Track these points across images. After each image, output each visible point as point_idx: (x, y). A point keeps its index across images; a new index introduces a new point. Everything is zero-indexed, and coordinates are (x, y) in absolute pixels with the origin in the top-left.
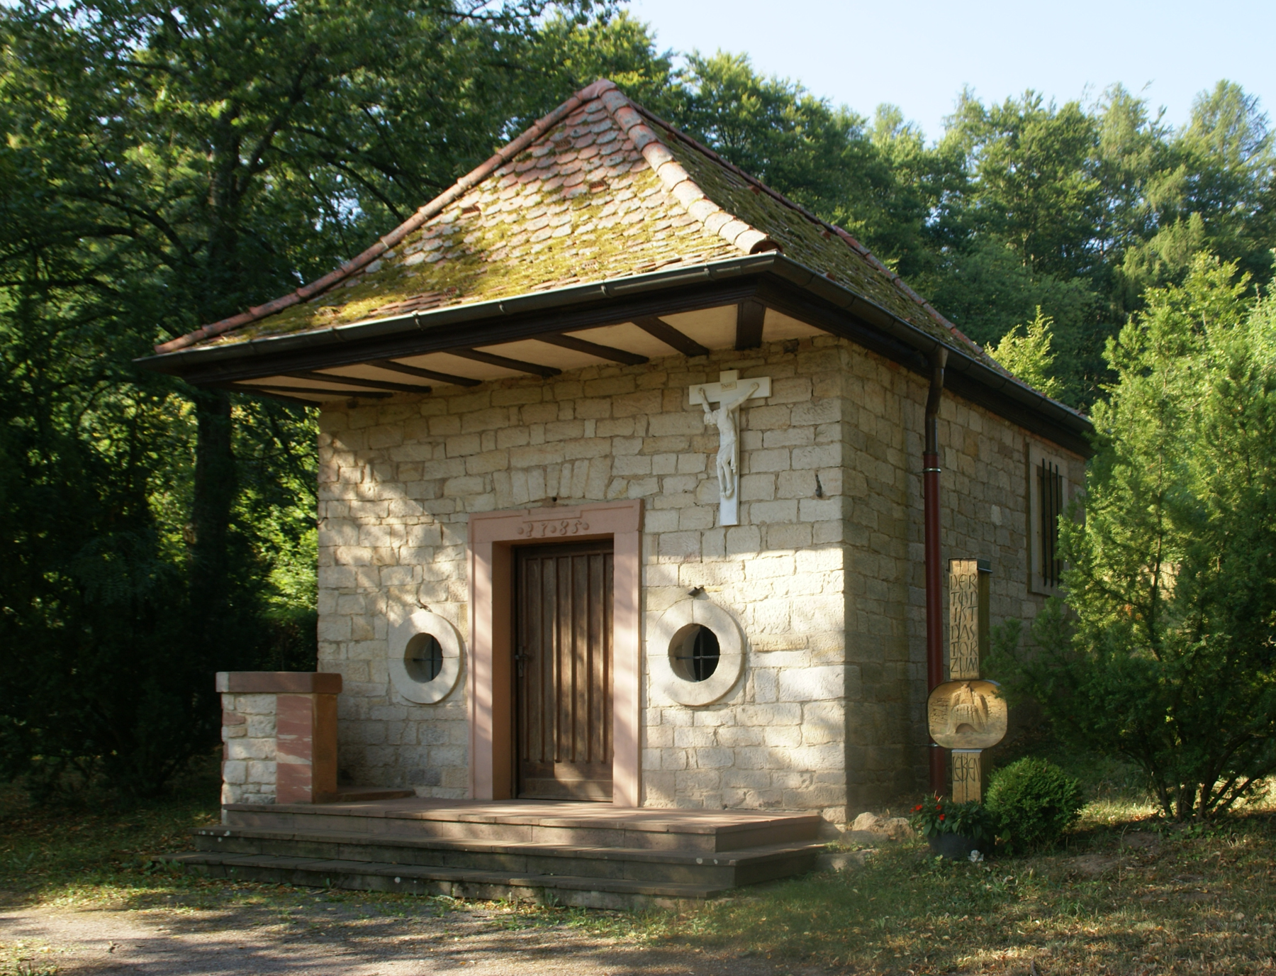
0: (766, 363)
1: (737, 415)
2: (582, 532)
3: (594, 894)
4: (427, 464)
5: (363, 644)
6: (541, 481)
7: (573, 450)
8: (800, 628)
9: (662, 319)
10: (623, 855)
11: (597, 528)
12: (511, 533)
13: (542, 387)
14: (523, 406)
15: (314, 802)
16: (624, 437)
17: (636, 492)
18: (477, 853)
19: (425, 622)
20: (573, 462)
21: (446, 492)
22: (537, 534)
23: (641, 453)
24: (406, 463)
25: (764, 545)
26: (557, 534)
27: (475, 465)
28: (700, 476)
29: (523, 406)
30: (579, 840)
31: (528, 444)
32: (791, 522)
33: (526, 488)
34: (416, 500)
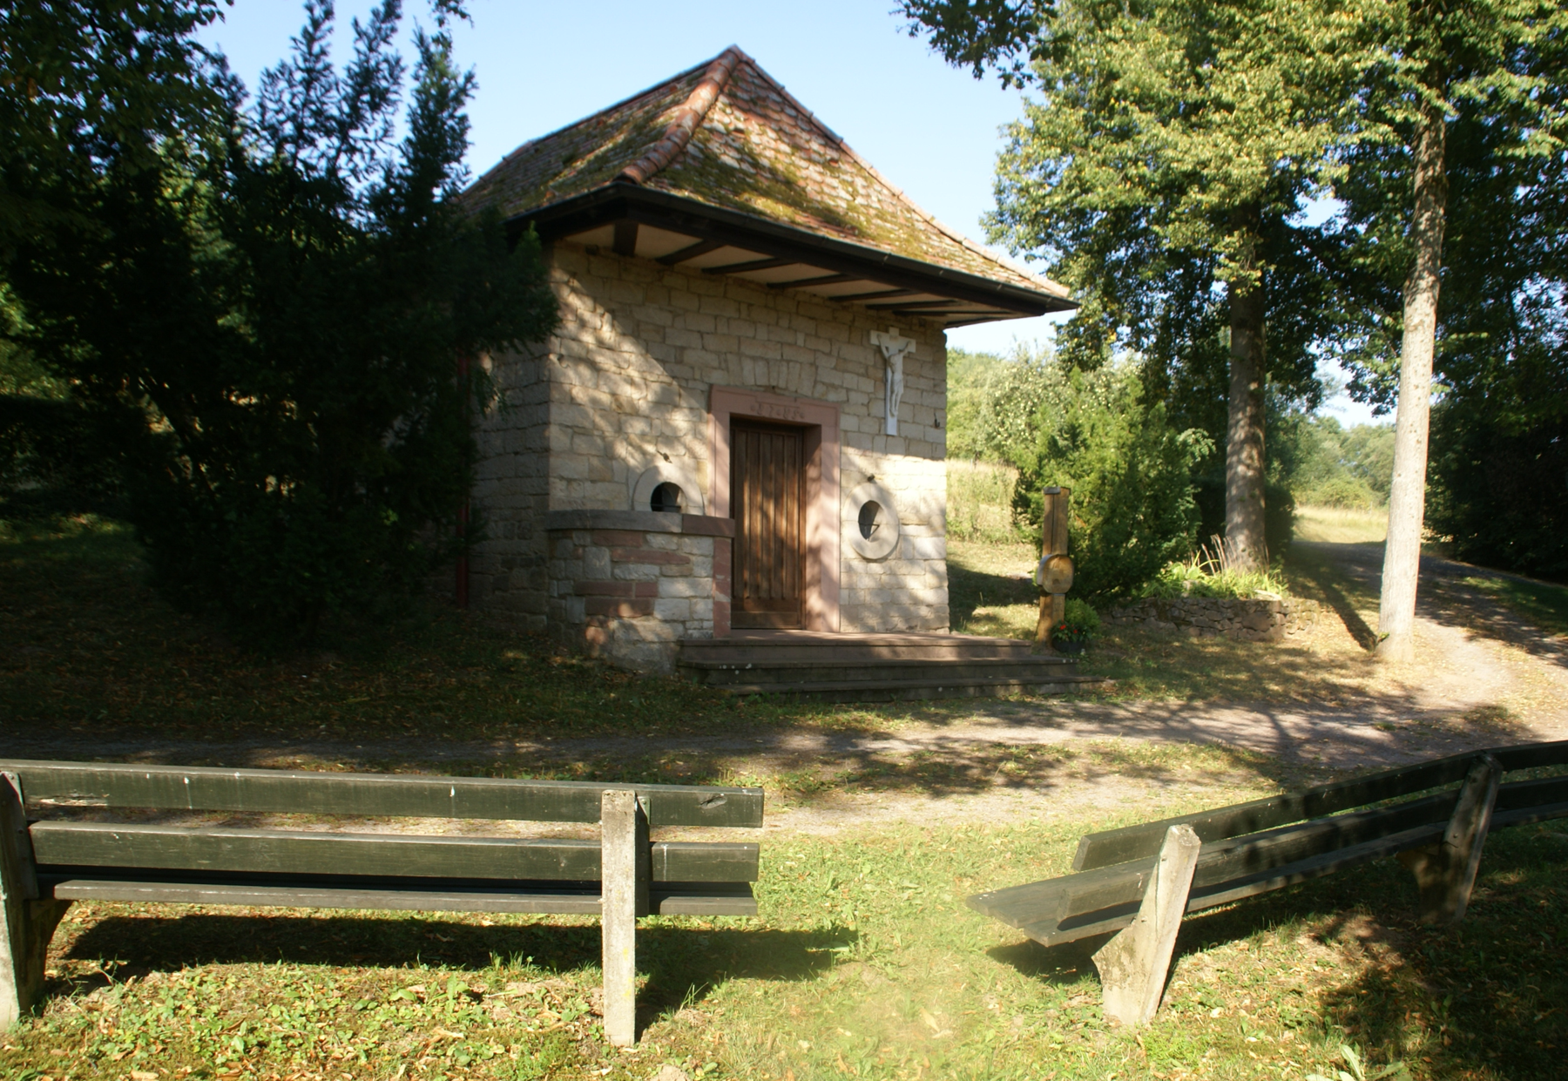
2: (799, 419)
4: (667, 330)
5: (599, 485)
7: (789, 352)
11: (809, 418)
12: (745, 408)
19: (669, 471)
23: (835, 368)
25: (907, 453)
26: (781, 417)
30: (959, 654)
31: (754, 338)
33: (753, 374)
34: (657, 359)
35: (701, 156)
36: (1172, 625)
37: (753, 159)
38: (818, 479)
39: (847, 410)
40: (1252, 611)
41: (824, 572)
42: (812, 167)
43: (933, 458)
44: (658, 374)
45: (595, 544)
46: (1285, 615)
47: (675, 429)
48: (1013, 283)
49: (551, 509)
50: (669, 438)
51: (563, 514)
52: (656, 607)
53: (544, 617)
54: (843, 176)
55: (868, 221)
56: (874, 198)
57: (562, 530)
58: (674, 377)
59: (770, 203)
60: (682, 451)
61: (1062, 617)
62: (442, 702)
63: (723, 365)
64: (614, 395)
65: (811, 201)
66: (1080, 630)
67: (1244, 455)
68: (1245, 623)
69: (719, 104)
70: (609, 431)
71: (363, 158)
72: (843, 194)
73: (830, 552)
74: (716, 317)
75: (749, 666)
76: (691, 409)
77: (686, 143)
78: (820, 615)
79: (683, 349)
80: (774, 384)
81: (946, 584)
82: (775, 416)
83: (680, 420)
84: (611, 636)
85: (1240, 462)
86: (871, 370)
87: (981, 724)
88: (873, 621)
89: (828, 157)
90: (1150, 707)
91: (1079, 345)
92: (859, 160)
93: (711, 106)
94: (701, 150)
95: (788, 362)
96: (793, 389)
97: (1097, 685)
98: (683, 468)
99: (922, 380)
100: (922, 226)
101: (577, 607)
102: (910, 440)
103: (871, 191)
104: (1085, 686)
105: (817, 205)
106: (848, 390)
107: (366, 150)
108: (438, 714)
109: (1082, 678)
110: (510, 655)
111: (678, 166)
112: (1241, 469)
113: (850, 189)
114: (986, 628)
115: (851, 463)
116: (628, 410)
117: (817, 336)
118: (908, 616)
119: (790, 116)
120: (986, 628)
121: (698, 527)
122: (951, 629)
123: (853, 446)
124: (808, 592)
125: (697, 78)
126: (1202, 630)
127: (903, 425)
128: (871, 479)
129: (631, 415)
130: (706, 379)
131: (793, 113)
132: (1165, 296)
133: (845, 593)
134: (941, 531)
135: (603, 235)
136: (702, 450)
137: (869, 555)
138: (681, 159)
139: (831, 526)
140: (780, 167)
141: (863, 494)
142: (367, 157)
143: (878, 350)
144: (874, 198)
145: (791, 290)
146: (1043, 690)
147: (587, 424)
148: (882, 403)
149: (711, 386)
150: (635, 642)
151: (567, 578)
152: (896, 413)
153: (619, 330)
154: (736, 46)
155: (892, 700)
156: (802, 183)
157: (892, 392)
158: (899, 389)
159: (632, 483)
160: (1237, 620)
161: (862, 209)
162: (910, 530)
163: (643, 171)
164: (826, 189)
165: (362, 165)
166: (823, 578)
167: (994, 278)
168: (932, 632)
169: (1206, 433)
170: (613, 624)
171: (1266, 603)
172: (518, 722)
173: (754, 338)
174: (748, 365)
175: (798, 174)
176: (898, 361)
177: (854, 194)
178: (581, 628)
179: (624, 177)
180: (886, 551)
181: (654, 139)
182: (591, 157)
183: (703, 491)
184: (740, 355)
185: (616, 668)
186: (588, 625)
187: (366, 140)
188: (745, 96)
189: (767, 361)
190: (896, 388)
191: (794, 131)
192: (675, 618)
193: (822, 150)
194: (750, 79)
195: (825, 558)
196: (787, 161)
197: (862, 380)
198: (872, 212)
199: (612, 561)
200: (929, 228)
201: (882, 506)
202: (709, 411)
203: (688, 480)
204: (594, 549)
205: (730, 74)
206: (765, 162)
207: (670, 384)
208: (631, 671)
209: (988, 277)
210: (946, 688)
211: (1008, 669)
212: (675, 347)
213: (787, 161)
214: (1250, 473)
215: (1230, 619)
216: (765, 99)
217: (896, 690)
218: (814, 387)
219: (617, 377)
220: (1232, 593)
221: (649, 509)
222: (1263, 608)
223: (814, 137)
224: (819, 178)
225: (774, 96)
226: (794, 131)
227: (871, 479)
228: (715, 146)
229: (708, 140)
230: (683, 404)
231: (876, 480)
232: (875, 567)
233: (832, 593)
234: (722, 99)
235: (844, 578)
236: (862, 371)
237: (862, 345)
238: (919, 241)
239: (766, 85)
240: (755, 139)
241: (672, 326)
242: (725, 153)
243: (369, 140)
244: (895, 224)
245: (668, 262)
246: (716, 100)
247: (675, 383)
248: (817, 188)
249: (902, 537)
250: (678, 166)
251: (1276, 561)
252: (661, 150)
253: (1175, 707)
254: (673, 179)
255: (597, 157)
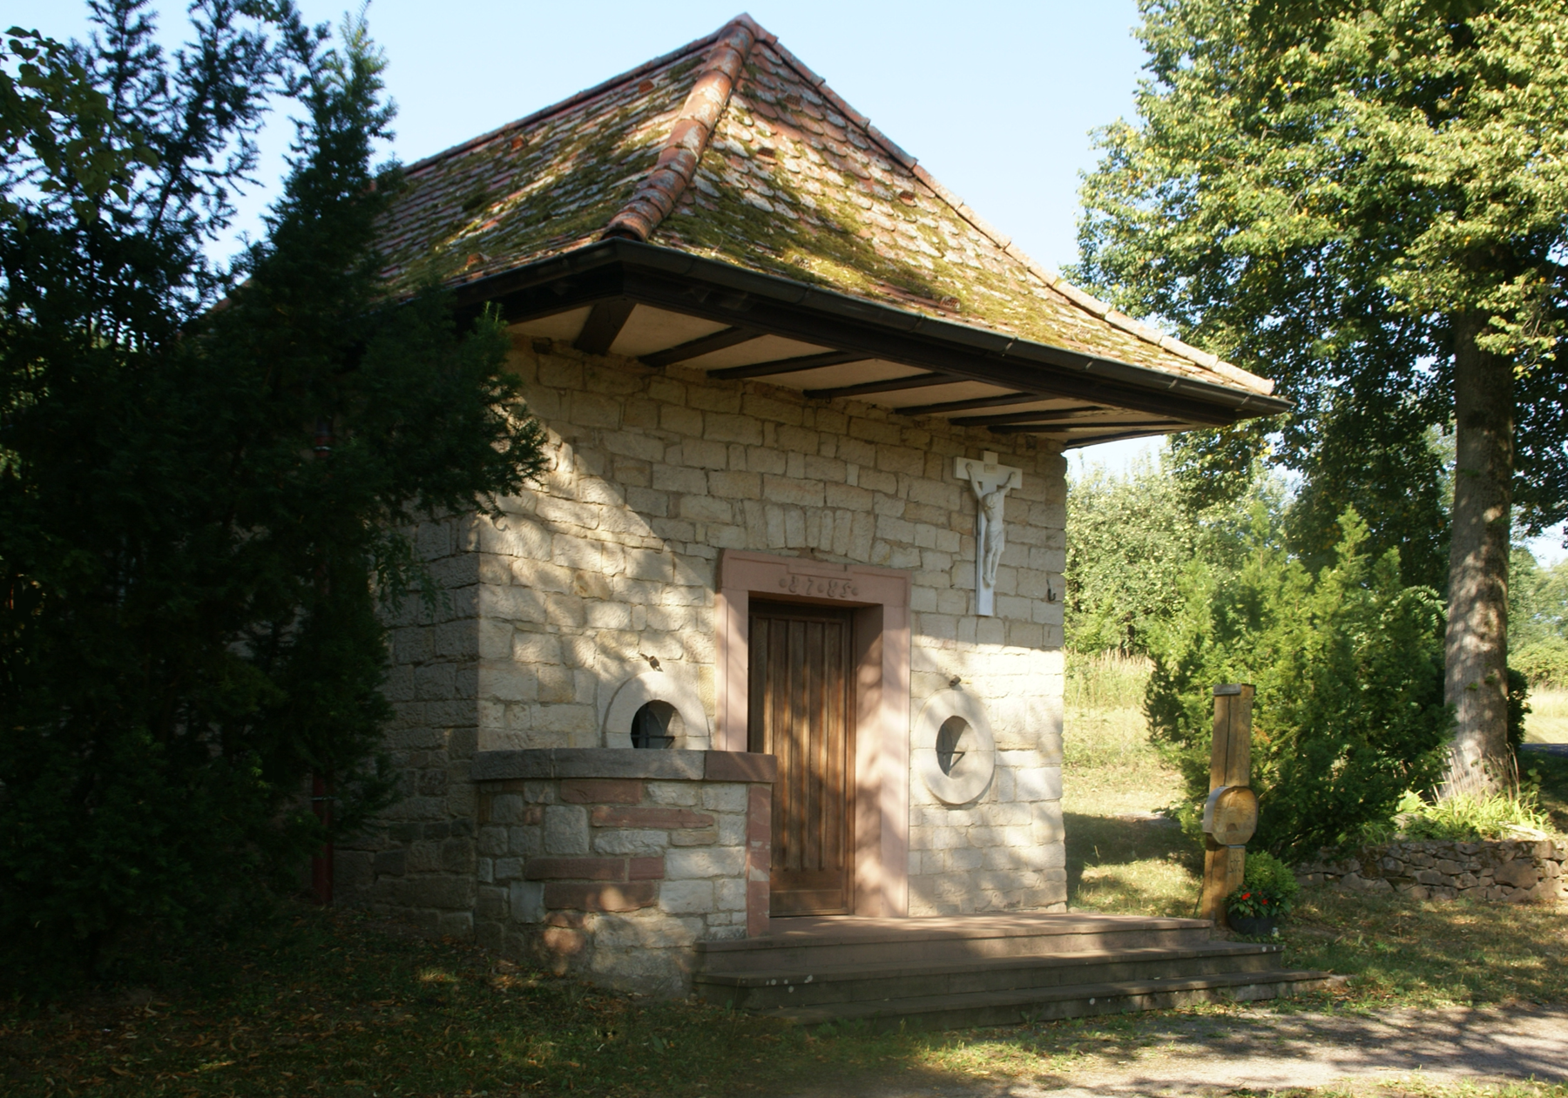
0: (1014, 453)
2: (850, 598)
3: (1252, 987)
4: (656, 467)
5: (553, 708)
6: (801, 524)
7: (835, 496)
8: (1030, 726)
9: (728, 326)
10: (1133, 955)
11: (865, 597)
12: (770, 585)
13: (804, 407)
14: (782, 425)
16: (886, 494)
19: (658, 685)
21: (683, 511)
22: (801, 590)
23: (902, 518)
24: (625, 457)
25: (1008, 641)
26: (824, 595)
27: (721, 484)
28: (959, 558)
29: (782, 425)
30: (1106, 944)
31: (784, 475)
32: (1026, 622)
33: (782, 530)
34: (639, 513)
35: (717, 194)
36: (1385, 884)
37: (791, 196)
38: (878, 684)
39: (920, 580)
40: (1509, 858)
41: (883, 822)
42: (877, 207)
43: (1044, 648)
44: (640, 532)
45: (564, 801)
46: (1559, 862)
47: (665, 617)
48: (1190, 376)
49: (481, 749)
50: (654, 632)
51: (507, 757)
52: (663, 894)
53: (469, 915)
54: (922, 220)
55: (966, 287)
56: (971, 253)
57: (503, 781)
58: (665, 540)
59: (828, 264)
60: (676, 651)
61: (1240, 881)
62: (354, 1061)
63: (739, 519)
64: (575, 569)
65: (881, 260)
66: (1271, 900)
67: (1475, 620)
68: (1499, 877)
69: (733, 111)
70: (567, 622)
71: (207, 203)
72: (926, 248)
73: (893, 793)
74: (728, 445)
75: (810, 979)
76: (690, 587)
77: (693, 173)
78: (878, 890)
79: (679, 495)
80: (813, 544)
81: (1062, 836)
82: (815, 593)
83: (672, 602)
84: (589, 941)
85: (1467, 630)
86: (956, 519)
87: (1180, 1055)
88: (956, 896)
89: (899, 191)
90: (1419, 1018)
91: (1214, 465)
92: (942, 194)
93: (723, 112)
94: (715, 184)
95: (834, 509)
96: (840, 550)
97: (1318, 984)
98: (677, 676)
99: (1030, 530)
100: (1044, 293)
101: (530, 900)
102: (1012, 621)
103: (964, 241)
104: (1300, 987)
105: (892, 267)
106: (922, 549)
107: (210, 189)
108: (356, 1082)
109: (1297, 974)
110: (429, 976)
111: (686, 211)
112: (1470, 641)
113: (935, 240)
114: (1109, 899)
115: (925, 659)
116: (597, 592)
117: (876, 469)
118: (1007, 885)
119: (836, 126)
120: (1109, 899)
121: (717, 769)
122: (1067, 904)
123: (928, 635)
124: (858, 856)
125: (687, 68)
126: (1432, 889)
127: (1001, 599)
128: (954, 683)
129: (601, 600)
130: (713, 542)
131: (840, 121)
132: (1335, 383)
133: (915, 857)
134: (1056, 756)
135: (567, 322)
136: (702, 645)
137: (952, 798)
138: (688, 199)
139: (895, 754)
140: (831, 208)
141: (943, 705)
142: (213, 201)
143: (967, 486)
144: (971, 253)
145: (840, 400)
146: (1241, 994)
147: (536, 616)
148: (971, 567)
149: (721, 551)
150: (627, 950)
151: (513, 854)
152: (993, 583)
153: (583, 470)
154: (746, 15)
155: (1023, 1022)
156: (865, 232)
157: (987, 551)
158: (998, 545)
159: (602, 704)
160: (1485, 872)
161: (955, 270)
162: (1010, 757)
163: (647, 220)
164: (902, 242)
165: (205, 216)
166: (882, 832)
167: (1163, 370)
168: (1041, 910)
169: (1434, 593)
170: (592, 922)
171: (1530, 845)
172: (486, 1088)
173: (784, 475)
174: (775, 516)
175: (857, 217)
176: (997, 503)
177: (941, 248)
178: (535, 931)
179: (621, 230)
180: (975, 790)
181: (636, 168)
182: (518, 197)
183: (707, 707)
184: (763, 502)
185: (600, 990)
186: (548, 925)
187: (211, 175)
188: (769, 96)
189: (803, 508)
190: (993, 544)
191: (845, 150)
192: (691, 910)
193: (887, 179)
194: (773, 69)
195: (886, 803)
196: (840, 197)
197: (943, 533)
198: (971, 274)
199: (592, 827)
200: (1054, 295)
201: (971, 723)
202: (718, 590)
203: (685, 694)
204: (562, 808)
205: (743, 60)
206: (808, 201)
207: (658, 551)
208: (623, 993)
209: (1154, 368)
210: (1099, 999)
211: (1185, 965)
212: (668, 493)
213: (840, 197)
214: (1485, 647)
215: (1474, 872)
216: (798, 100)
217: (1027, 1006)
218: (872, 547)
219: (581, 542)
220: (1473, 831)
221: (630, 744)
222: (1525, 851)
223: (874, 159)
224: (888, 224)
225: (810, 95)
226: (845, 150)
227: (954, 683)
228: (733, 178)
229: (723, 168)
230: (679, 580)
231: (962, 684)
232: (959, 816)
233: (898, 855)
234: (736, 101)
235: (914, 834)
236: (943, 520)
237: (942, 480)
238: (1044, 317)
239: (796, 78)
240: (790, 164)
241: (663, 461)
242: (749, 189)
243: (218, 175)
244: (1004, 291)
245: (657, 361)
246: (728, 104)
247: (666, 548)
248: (887, 239)
249: (1000, 768)
250: (686, 211)
251: (1529, 778)
252: (660, 185)
253: (1458, 1017)
254: (687, 232)
255: (531, 200)
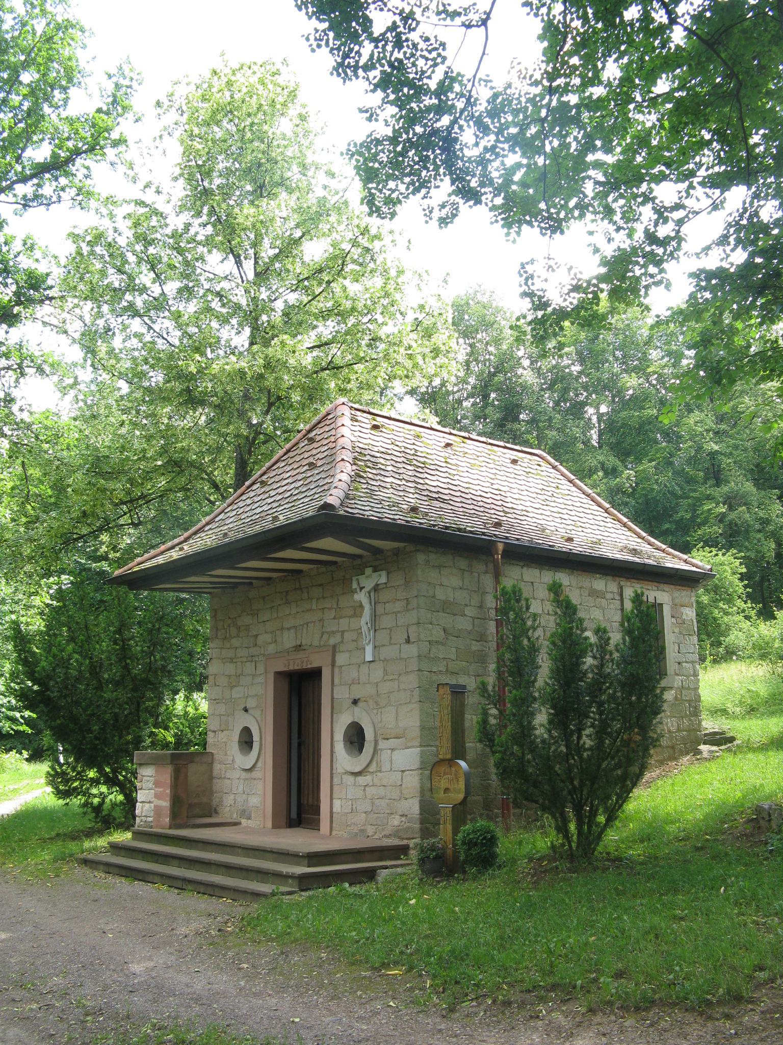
1: (372, 594)
15: (170, 828)
17: (332, 641)
18: (364, 852)
20: (307, 624)
23: (334, 618)
33: (288, 640)
